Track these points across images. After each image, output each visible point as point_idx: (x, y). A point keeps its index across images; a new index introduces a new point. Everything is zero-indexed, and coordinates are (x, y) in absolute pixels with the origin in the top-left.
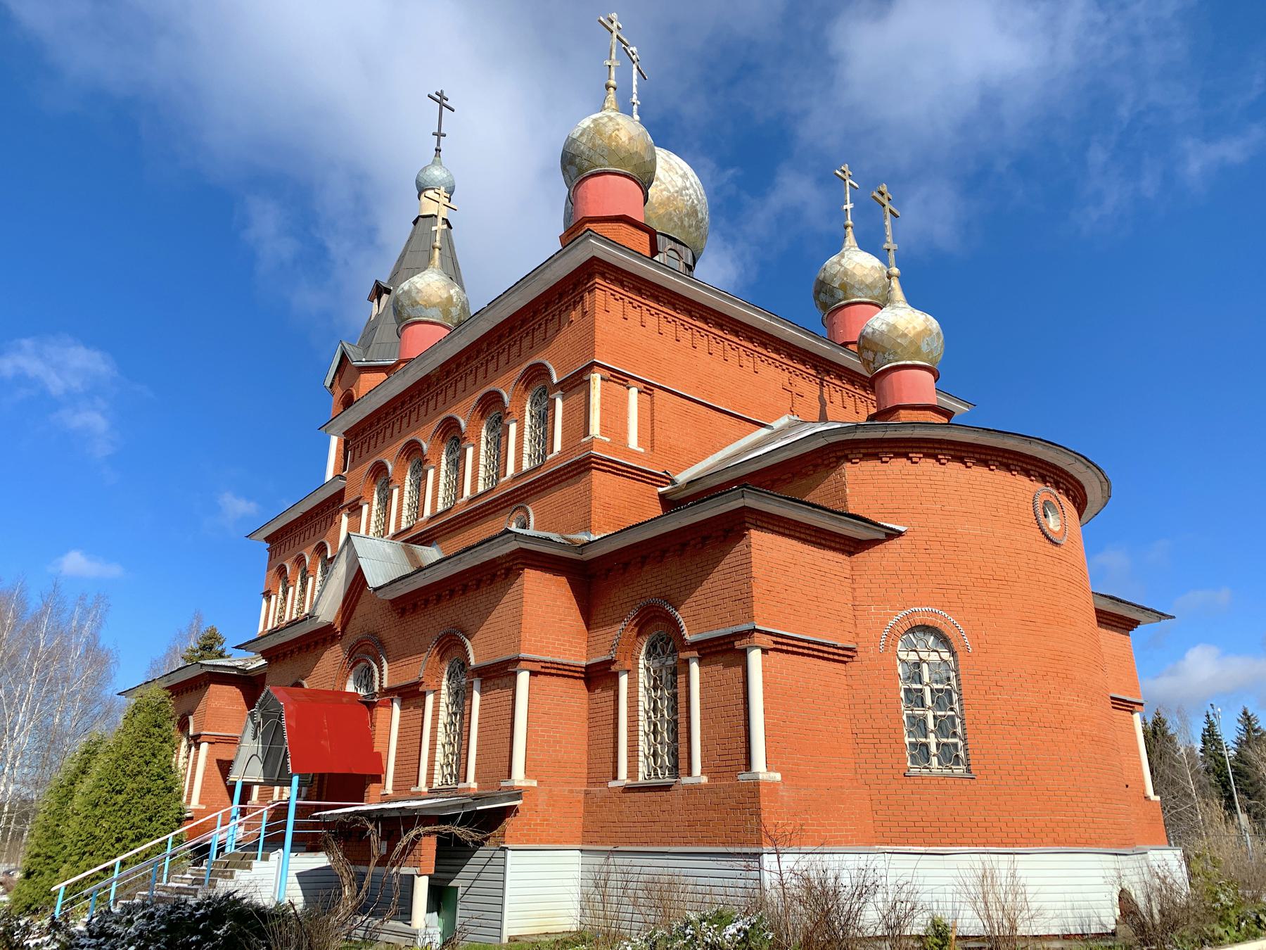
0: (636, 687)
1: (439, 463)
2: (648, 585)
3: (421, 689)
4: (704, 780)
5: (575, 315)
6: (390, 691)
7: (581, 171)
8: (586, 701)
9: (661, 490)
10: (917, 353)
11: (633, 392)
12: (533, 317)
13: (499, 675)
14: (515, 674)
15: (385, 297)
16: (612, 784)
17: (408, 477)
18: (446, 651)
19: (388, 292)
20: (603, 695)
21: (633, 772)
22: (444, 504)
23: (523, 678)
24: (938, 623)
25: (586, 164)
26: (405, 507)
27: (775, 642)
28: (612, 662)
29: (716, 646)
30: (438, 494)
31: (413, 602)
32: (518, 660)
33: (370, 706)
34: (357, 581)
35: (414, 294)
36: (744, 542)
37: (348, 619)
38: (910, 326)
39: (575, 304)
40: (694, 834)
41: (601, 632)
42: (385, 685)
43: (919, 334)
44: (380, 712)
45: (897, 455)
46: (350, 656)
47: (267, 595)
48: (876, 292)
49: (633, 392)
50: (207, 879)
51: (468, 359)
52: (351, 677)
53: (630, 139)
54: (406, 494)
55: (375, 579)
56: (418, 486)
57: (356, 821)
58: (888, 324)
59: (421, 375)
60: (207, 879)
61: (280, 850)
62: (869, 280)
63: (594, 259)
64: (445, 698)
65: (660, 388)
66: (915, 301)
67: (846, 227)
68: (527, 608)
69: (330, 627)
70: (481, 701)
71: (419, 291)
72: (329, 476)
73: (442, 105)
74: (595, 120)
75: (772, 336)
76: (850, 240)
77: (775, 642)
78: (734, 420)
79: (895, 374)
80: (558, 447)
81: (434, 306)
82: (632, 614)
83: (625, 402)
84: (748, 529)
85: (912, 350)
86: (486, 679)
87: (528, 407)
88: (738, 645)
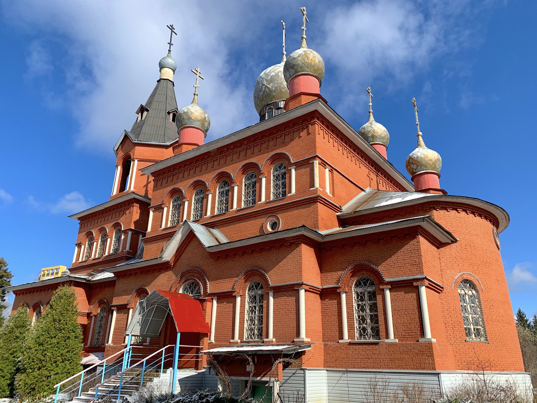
2: (359, 256)
4: (112, 345)
5: (303, 134)
9: (337, 214)
10: (434, 168)
11: (327, 170)
13: (292, 290)
15: (145, 113)
16: (123, 344)
18: (249, 277)
19: (147, 111)
20: (332, 303)
21: (351, 336)
22: (218, 211)
23: (302, 293)
24: (472, 279)
25: (300, 69)
27: (429, 284)
32: (302, 284)
33: (202, 301)
35: (189, 114)
36: (415, 240)
37: (178, 260)
39: (303, 129)
40: (395, 364)
43: (436, 160)
44: (208, 304)
45: (453, 209)
47: (79, 245)
48: (385, 140)
49: (327, 170)
50: (142, 382)
51: (234, 147)
53: (319, 62)
57: (237, 355)
58: (424, 155)
59: (206, 151)
60: (142, 382)
61: (171, 368)
62: (383, 136)
63: (316, 111)
66: (429, 146)
67: (370, 112)
69: (167, 263)
70: (274, 301)
71: (192, 113)
73: (172, 31)
74: (304, 51)
75: (365, 153)
76: (372, 118)
77: (429, 284)
79: (426, 175)
80: (293, 191)
81: (199, 121)
82: (350, 268)
83: (324, 174)
84: (418, 235)
85: (433, 166)
86: (277, 292)
88: (415, 284)
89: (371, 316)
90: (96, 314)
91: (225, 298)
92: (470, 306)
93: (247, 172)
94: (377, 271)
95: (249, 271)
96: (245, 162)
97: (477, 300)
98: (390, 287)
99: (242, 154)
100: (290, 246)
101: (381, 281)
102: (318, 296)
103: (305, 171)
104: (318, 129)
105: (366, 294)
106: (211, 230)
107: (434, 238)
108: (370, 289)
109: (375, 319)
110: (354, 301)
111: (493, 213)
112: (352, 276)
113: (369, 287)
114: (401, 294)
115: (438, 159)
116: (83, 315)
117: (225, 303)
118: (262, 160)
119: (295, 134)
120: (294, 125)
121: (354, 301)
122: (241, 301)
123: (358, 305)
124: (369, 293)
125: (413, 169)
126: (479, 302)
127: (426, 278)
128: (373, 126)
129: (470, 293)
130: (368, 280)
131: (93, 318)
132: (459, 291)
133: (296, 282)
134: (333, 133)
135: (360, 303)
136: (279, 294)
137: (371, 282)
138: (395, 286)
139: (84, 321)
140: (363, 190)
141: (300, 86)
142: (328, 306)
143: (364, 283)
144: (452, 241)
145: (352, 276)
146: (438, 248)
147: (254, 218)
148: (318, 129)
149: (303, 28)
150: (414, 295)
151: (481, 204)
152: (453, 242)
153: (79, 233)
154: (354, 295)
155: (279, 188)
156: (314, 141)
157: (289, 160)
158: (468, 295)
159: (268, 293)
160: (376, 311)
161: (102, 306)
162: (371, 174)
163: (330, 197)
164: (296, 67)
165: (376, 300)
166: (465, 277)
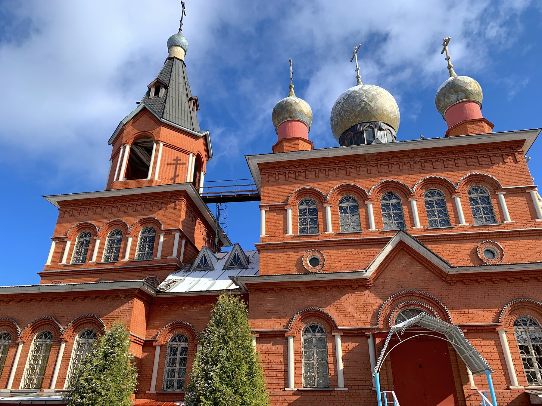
21: (297, 384)
90: (163, 343)
93: (428, 188)
96: (428, 176)
106: (424, 244)
109: (43, 369)
116: (136, 341)
117: (479, 339)
131: (158, 350)
138: (348, 335)
139: (137, 351)
141: (473, 112)
147: (457, 242)
151: (106, 266)
153: (59, 222)
161: (176, 332)
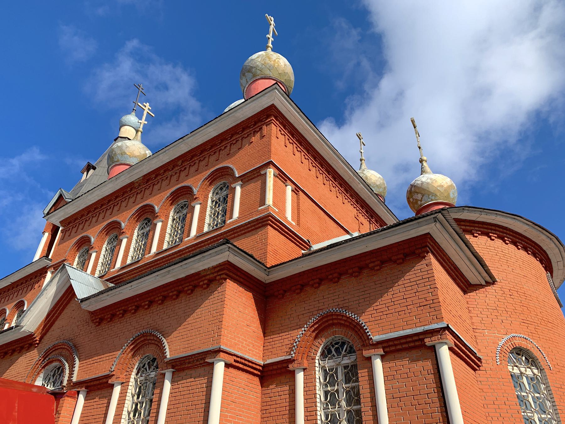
0: (310, 385)
1: (132, 235)
2: (327, 300)
3: (110, 382)
5: (255, 139)
6: (79, 384)
7: (254, 75)
8: (259, 395)
9: (303, 252)
12: (220, 143)
13: (195, 365)
14: (212, 365)
15: (91, 171)
17: (105, 246)
19: (94, 168)
20: (278, 391)
23: (219, 368)
24: (529, 347)
25: (259, 72)
26: (100, 264)
27: (456, 345)
28: (291, 361)
29: (401, 344)
30: (128, 251)
31: (105, 316)
32: (219, 351)
33: (58, 395)
34: (68, 294)
35: (124, 148)
36: (424, 262)
37: (47, 331)
38: (444, 182)
39: (255, 132)
41: (276, 337)
42: (74, 379)
44: (66, 402)
45: (483, 234)
46: (45, 357)
49: (289, 189)
52: (42, 375)
54: (102, 256)
55: (81, 292)
56: (112, 250)
59: (128, 182)
62: (378, 183)
64: (131, 389)
65: (303, 191)
68: (227, 310)
69: (30, 336)
70: (172, 389)
71: (127, 147)
72: (37, 257)
78: (335, 225)
81: (135, 157)
83: (284, 193)
84: (428, 252)
85: (446, 194)
86: (178, 370)
87: (210, 195)
89: (349, 412)
91: (99, 389)
92: (533, 398)
93: (178, 201)
94: (358, 324)
95: (139, 337)
97: (543, 386)
98: (382, 353)
99: (175, 178)
100: (208, 285)
101: (367, 343)
102: (257, 380)
103: (254, 186)
104: (274, 130)
105: (339, 370)
107: (456, 269)
108: (346, 361)
110: (318, 384)
111: (544, 248)
112: (316, 337)
113: (345, 356)
114: (403, 364)
115: (452, 185)
118: (196, 182)
119: (244, 140)
120: (244, 129)
121: (318, 384)
122: (121, 393)
123: (326, 393)
124: (346, 367)
125: (417, 200)
126: (547, 388)
127: (448, 328)
128: (365, 172)
129: (529, 372)
130: (343, 344)
132: (510, 368)
133: (210, 348)
134: (301, 145)
135: (329, 389)
136: (182, 374)
137: (347, 342)
138: (392, 349)
140: (348, 232)
142: (273, 399)
143: (337, 350)
144: (486, 282)
145: (316, 337)
146: (465, 292)
148: (274, 130)
149: (268, 36)
150: (428, 365)
152: (488, 284)
154: (319, 375)
155: (218, 217)
156: (269, 144)
157: (233, 174)
158: (527, 377)
159: (164, 375)
160: (358, 402)
162: (360, 215)
163: (291, 224)
164: (254, 70)
165: (357, 380)
166: (518, 342)
